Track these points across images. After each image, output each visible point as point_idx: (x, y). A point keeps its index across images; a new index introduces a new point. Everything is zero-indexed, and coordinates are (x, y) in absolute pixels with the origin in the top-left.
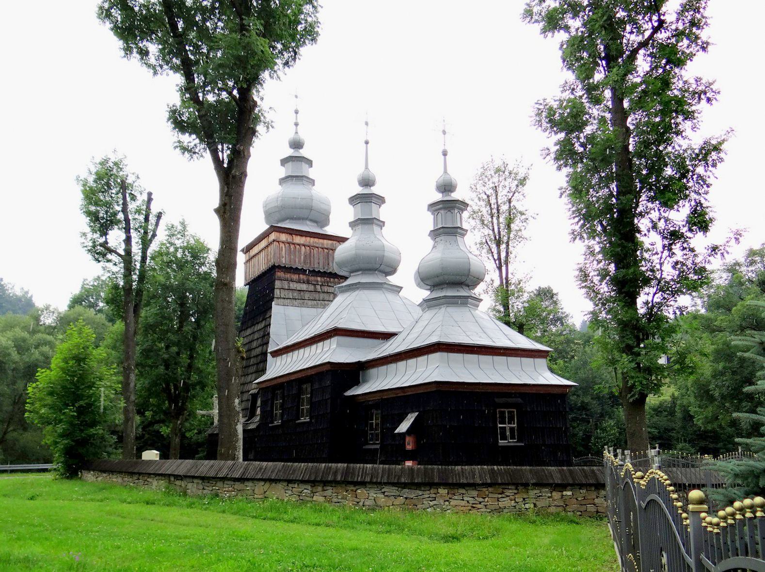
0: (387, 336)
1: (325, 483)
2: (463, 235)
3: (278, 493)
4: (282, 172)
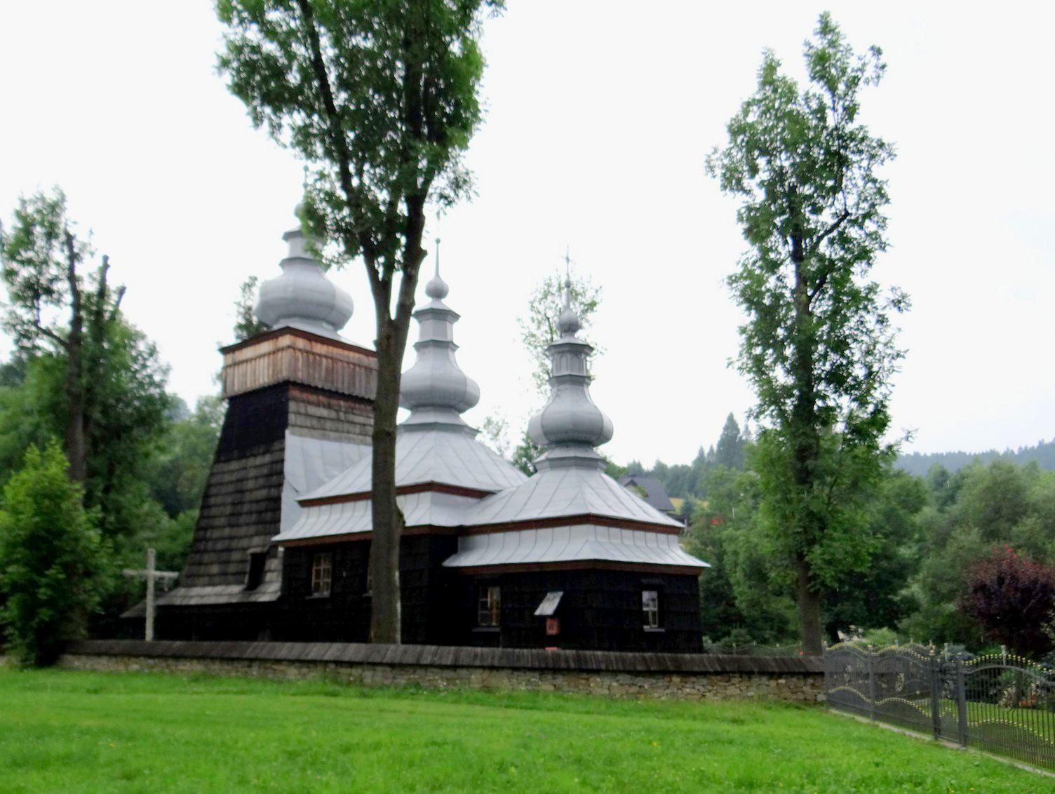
0: (481, 495)
1: (556, 671)
2: (454, 351)
3: (503, 682)
4: (285, 250)
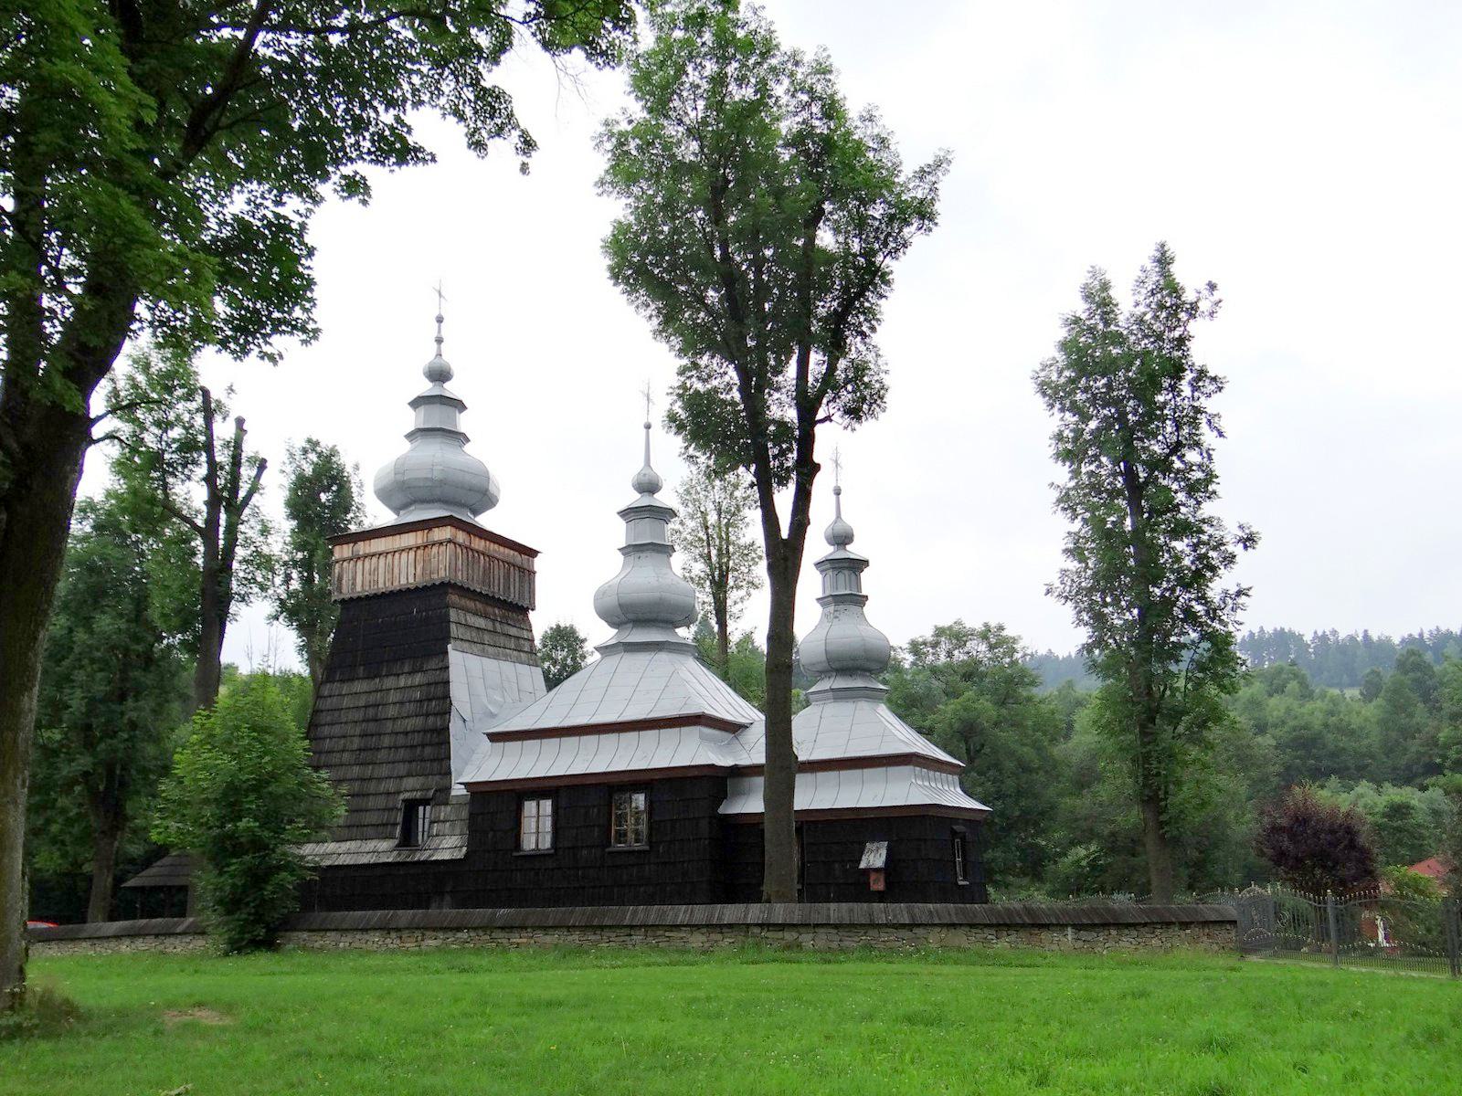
3: (960, 938)
4: (411, 420)
